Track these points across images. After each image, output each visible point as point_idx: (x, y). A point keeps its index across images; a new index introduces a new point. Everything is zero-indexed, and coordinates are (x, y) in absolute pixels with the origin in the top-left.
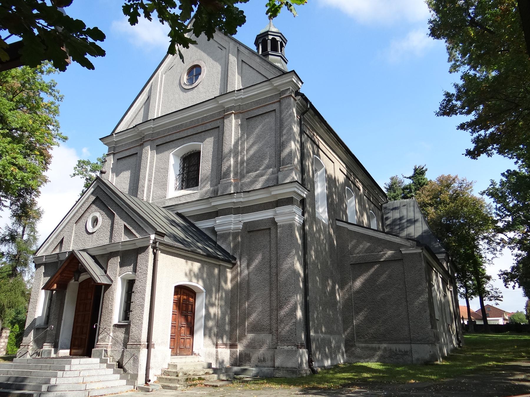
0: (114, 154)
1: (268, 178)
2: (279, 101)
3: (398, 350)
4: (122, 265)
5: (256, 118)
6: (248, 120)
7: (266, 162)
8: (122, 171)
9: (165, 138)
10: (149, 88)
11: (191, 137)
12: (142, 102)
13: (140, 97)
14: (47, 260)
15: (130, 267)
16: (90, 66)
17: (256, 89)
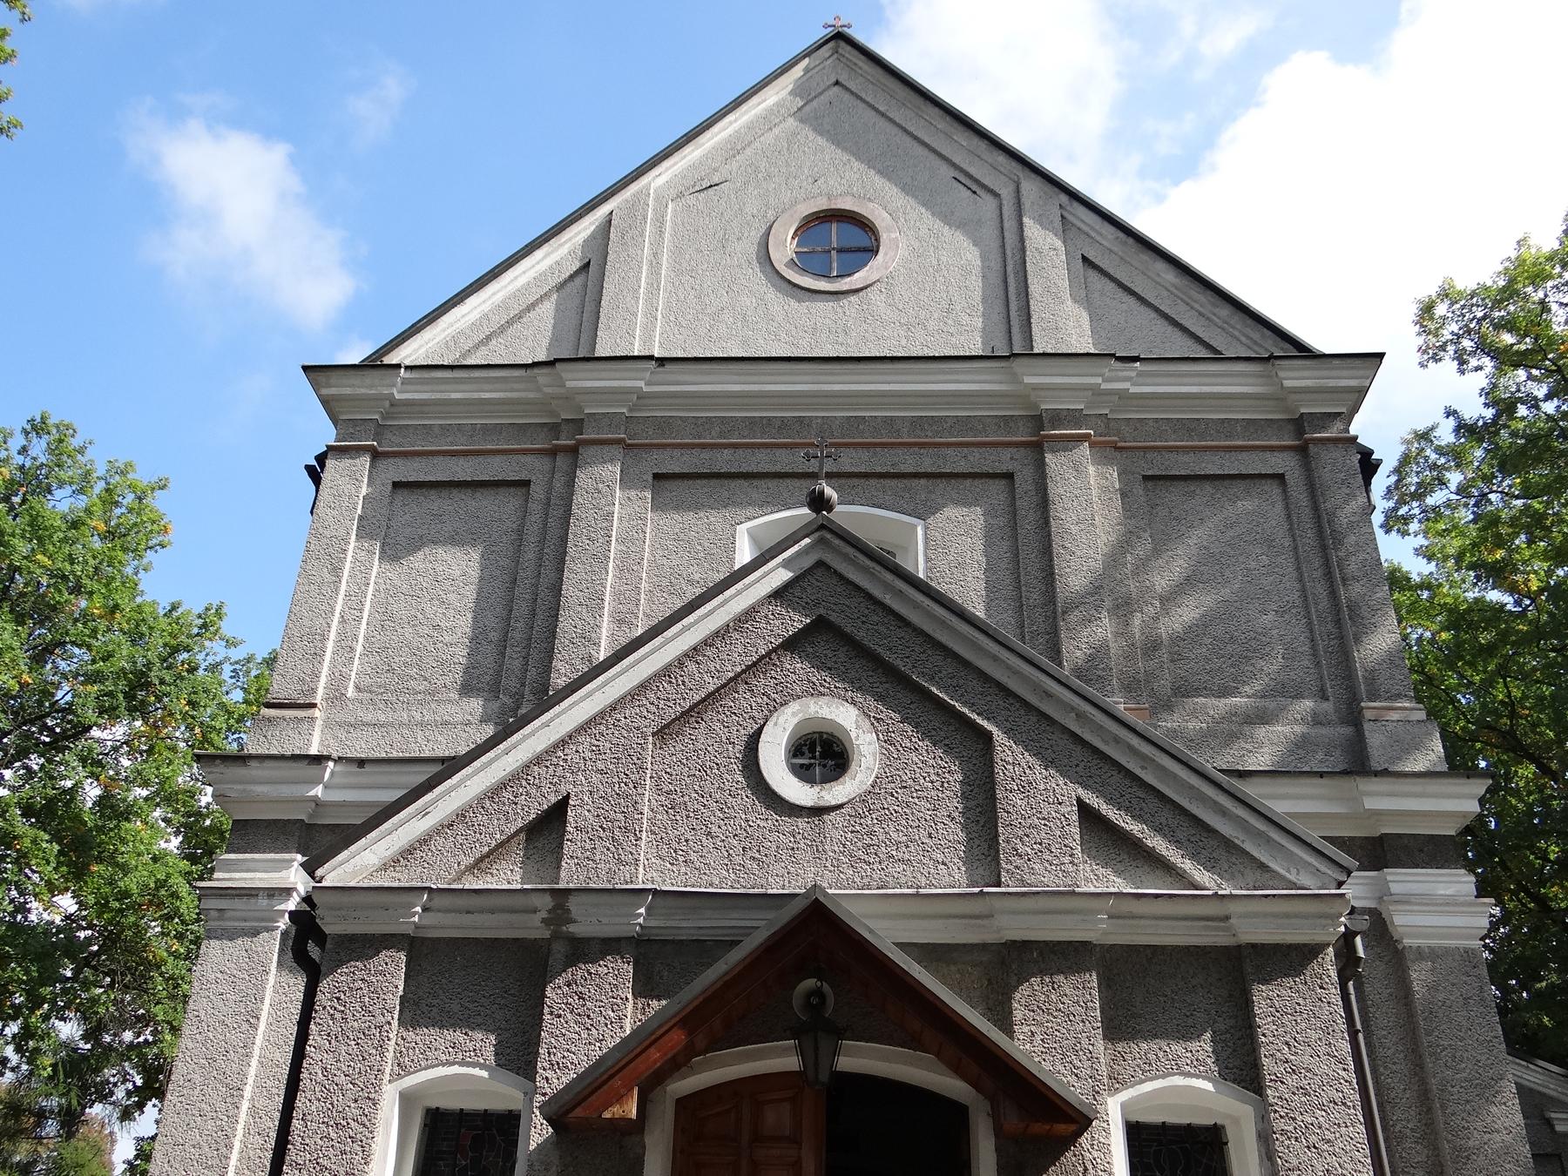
0: (376, 455)
1: (1304, 736)
4: (415, 1012)
7: (1272, 666)
8: (423, 545)
9: (706, 455)
10: (589, 232)
11: (855, 481)
12: (543, 274)
13: (539, 254)
14: (431, 919)
15: (1194, 1045)
17: (1199, 375)
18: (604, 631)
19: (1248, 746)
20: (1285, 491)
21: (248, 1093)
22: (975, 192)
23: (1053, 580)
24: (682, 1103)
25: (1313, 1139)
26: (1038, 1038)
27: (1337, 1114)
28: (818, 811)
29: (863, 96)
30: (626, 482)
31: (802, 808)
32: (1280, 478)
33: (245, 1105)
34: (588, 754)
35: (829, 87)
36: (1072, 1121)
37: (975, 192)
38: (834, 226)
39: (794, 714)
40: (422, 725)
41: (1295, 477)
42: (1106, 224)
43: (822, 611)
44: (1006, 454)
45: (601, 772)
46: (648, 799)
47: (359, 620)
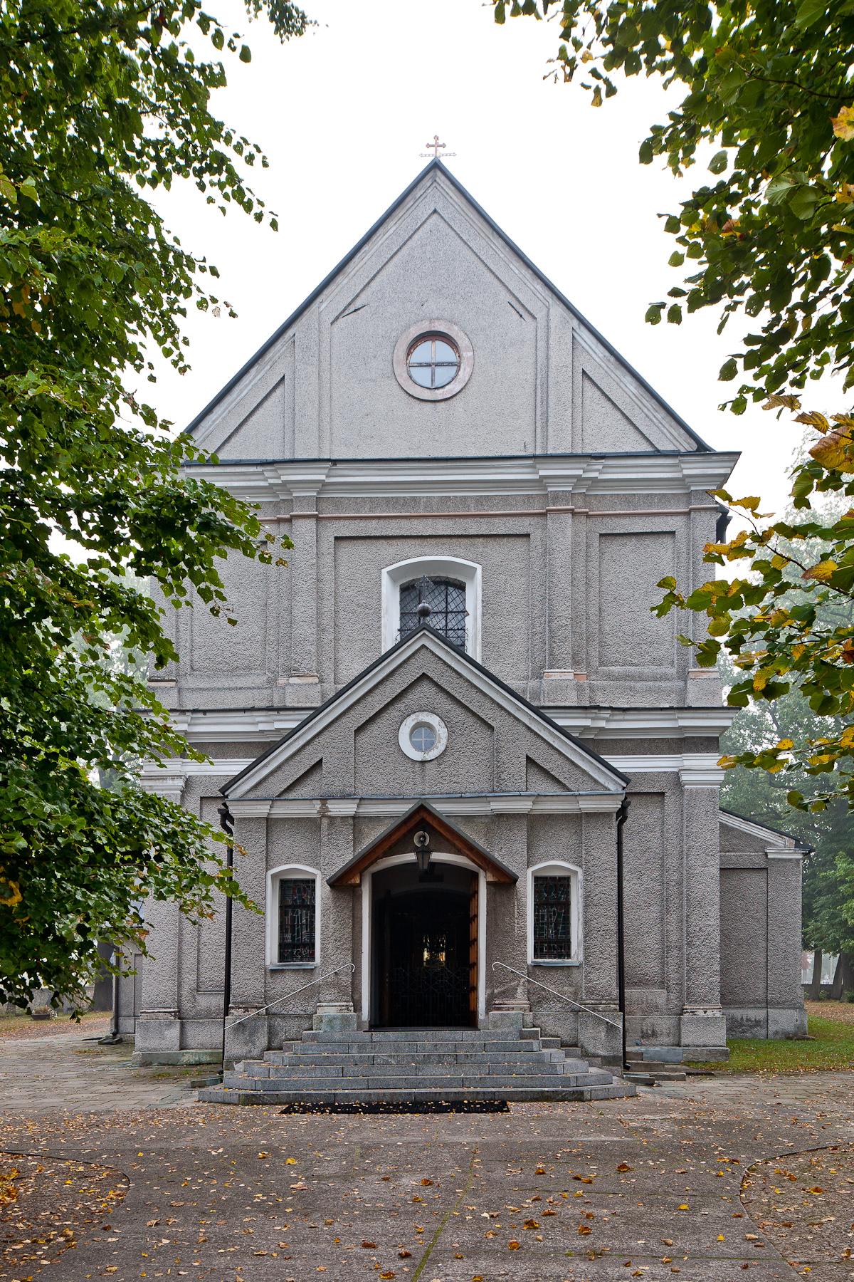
2: (688, 514)
3: (744, 1018)
5: (625, 540)
9: (362, 524)
13: (253, 371)
28: (423, 762)
35: (430, 216)
37: (521, 316)
42: (599, 345)
43: (424, 671)
44: (527, 521)
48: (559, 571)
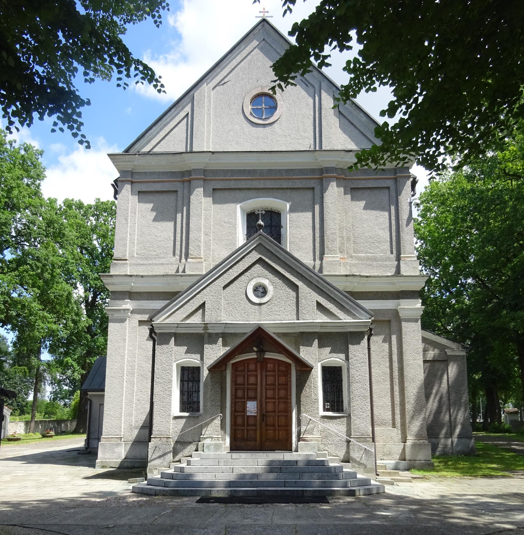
0: (132, 183)
6: (352, 190)
9: (227, 182)
16: (392, 92)
18: (202, 238)
19: (371, 268)
20: (389, 192)
21: (126, 357)
22: (307, 86)
23: (324, 221)
24: (233, 364)
25: (357, 369)
26: (305, 351)
27: (362, 364)
28: (260, 304)
29: (272, 45)
30: (205, 195)
31: (257, 303)
32: (388, 188)
33: (126, 360)
34: (209, 292)
36: (310, 368)
37: (307, 86)
38: (263, 98)
39: (254, 282)
40: (156, 264)
41: (392, 188)
44: (313, 181)
45: (212, 296)
46: (223, 302)
47: (134, 234)
48: (330, 206)
